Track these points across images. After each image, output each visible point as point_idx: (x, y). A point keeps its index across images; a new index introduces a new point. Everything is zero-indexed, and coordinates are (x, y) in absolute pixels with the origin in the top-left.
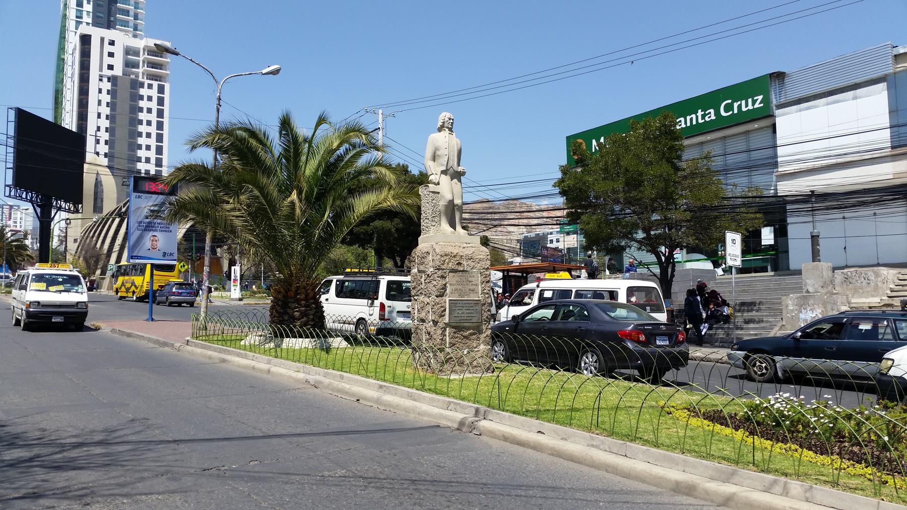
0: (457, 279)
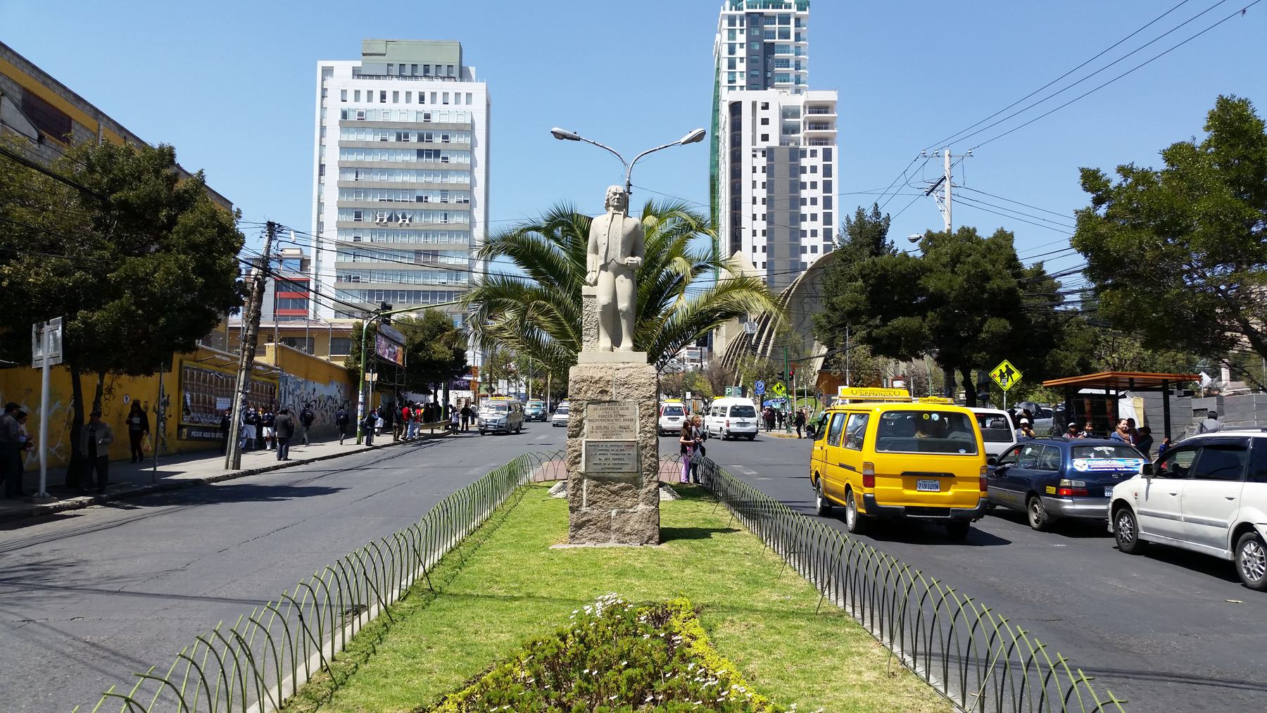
0: (601, 412)
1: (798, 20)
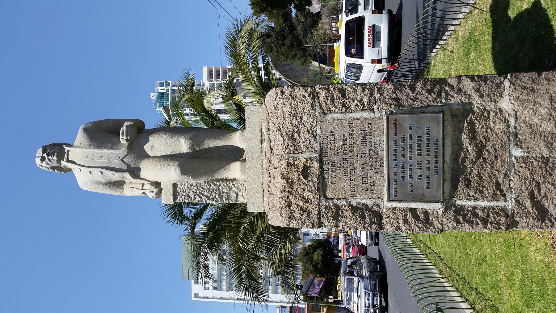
0: (339, 176)
1: (173, 86)
